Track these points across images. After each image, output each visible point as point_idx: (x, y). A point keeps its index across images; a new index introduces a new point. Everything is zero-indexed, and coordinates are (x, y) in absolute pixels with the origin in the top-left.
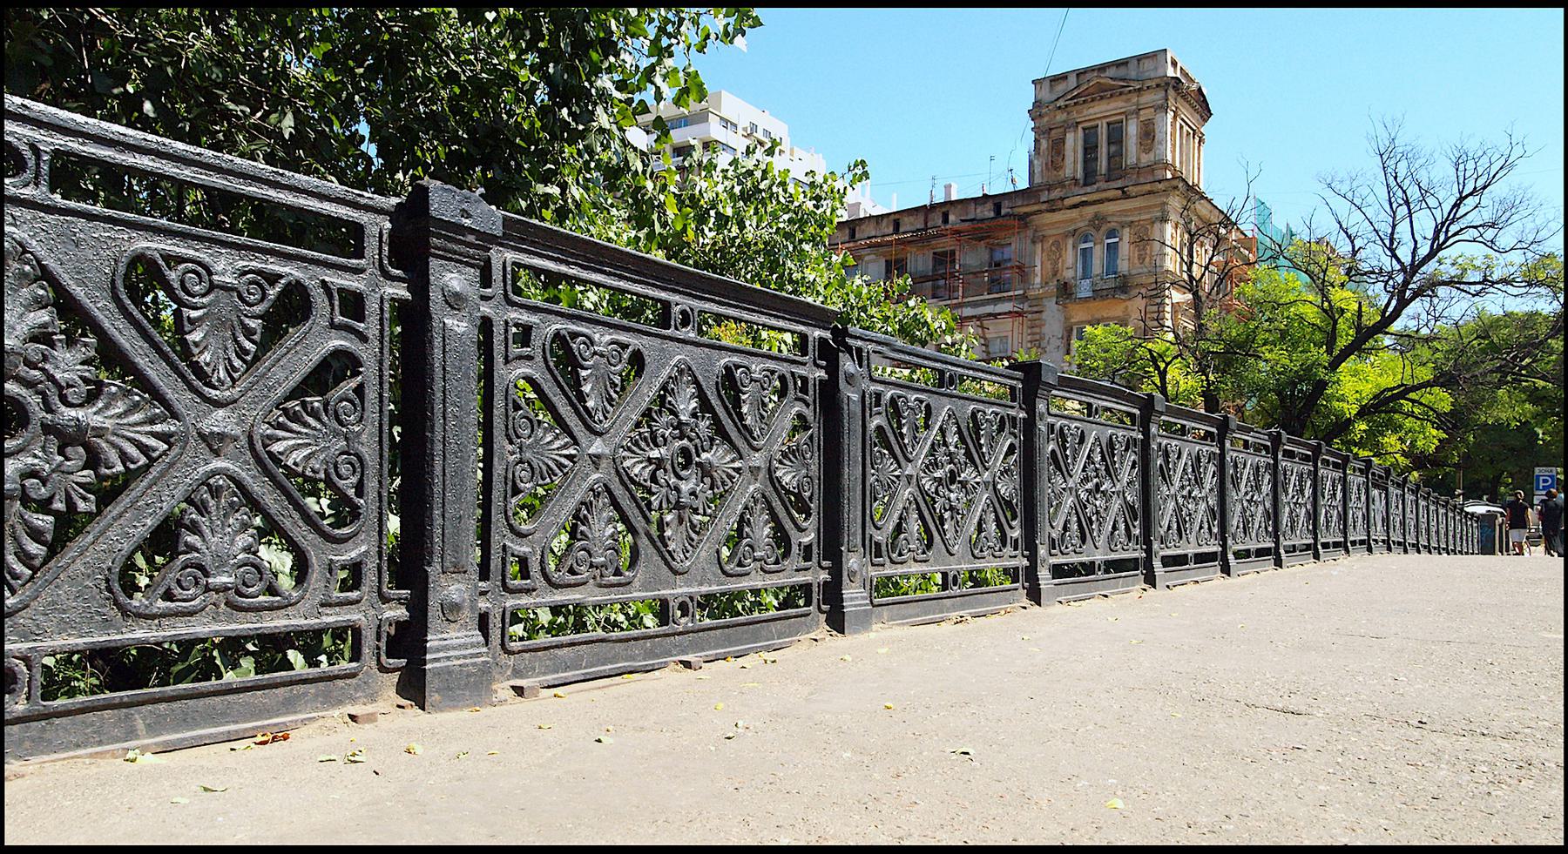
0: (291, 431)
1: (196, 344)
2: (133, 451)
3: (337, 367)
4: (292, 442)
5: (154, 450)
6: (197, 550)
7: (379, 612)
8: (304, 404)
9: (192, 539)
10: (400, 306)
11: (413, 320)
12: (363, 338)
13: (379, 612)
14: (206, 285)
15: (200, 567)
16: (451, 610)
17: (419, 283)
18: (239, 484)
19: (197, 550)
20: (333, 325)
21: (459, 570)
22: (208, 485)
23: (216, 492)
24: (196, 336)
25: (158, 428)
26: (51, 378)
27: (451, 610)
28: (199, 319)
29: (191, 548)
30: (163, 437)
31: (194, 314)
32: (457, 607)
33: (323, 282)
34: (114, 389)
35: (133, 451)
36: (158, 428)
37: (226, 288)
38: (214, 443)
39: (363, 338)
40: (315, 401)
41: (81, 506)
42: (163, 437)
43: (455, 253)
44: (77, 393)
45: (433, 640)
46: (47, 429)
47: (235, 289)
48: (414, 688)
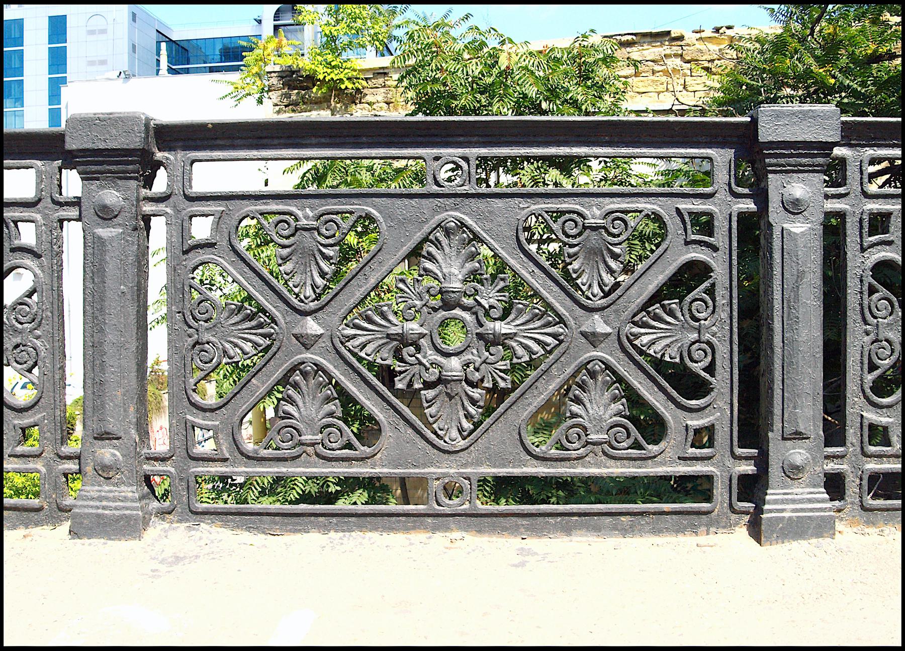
0: (655, 328)
1: (575, 271)
2: (535, 347)
3: (692, 275)
4: (655, 336)
5: (548, 345)
6: (581, 417)
7: (726, 466)
8: (663, 306)
9: (575, 408)
10: (743, 217)
11: (753, 234)
12: (715, 249)
13: (726, 466)
14: (580, 227)
15: (585, 429)
16: (793, 472)
17: (761, 196)
18: (608, 367)
19: (581, 417)
20: (687, 243)
21: (798, 436)
22: (587, 369)
23: (593, 375)
24: (576, 265)
25: (549, 330)
26: (479, 304)
27: (793, 472)
28: (575, 254)
29: (574, 415)
30: (555, 336)
31: (572, 250)
32: (798, 469)
33: (677, 208)
34: (521, 306)
35: (535, 347)
36: (549, 330)
37: (595, 228)
38: (593, 339)
39: (715, 249)
40: (674, 304)
41: (502, 384)
42: (555, 336)
43: (804, 166)
44: (495, 313)
45: (772, 494)
46: (480, 336)
47: (604, 228)
48: (756, 530)
